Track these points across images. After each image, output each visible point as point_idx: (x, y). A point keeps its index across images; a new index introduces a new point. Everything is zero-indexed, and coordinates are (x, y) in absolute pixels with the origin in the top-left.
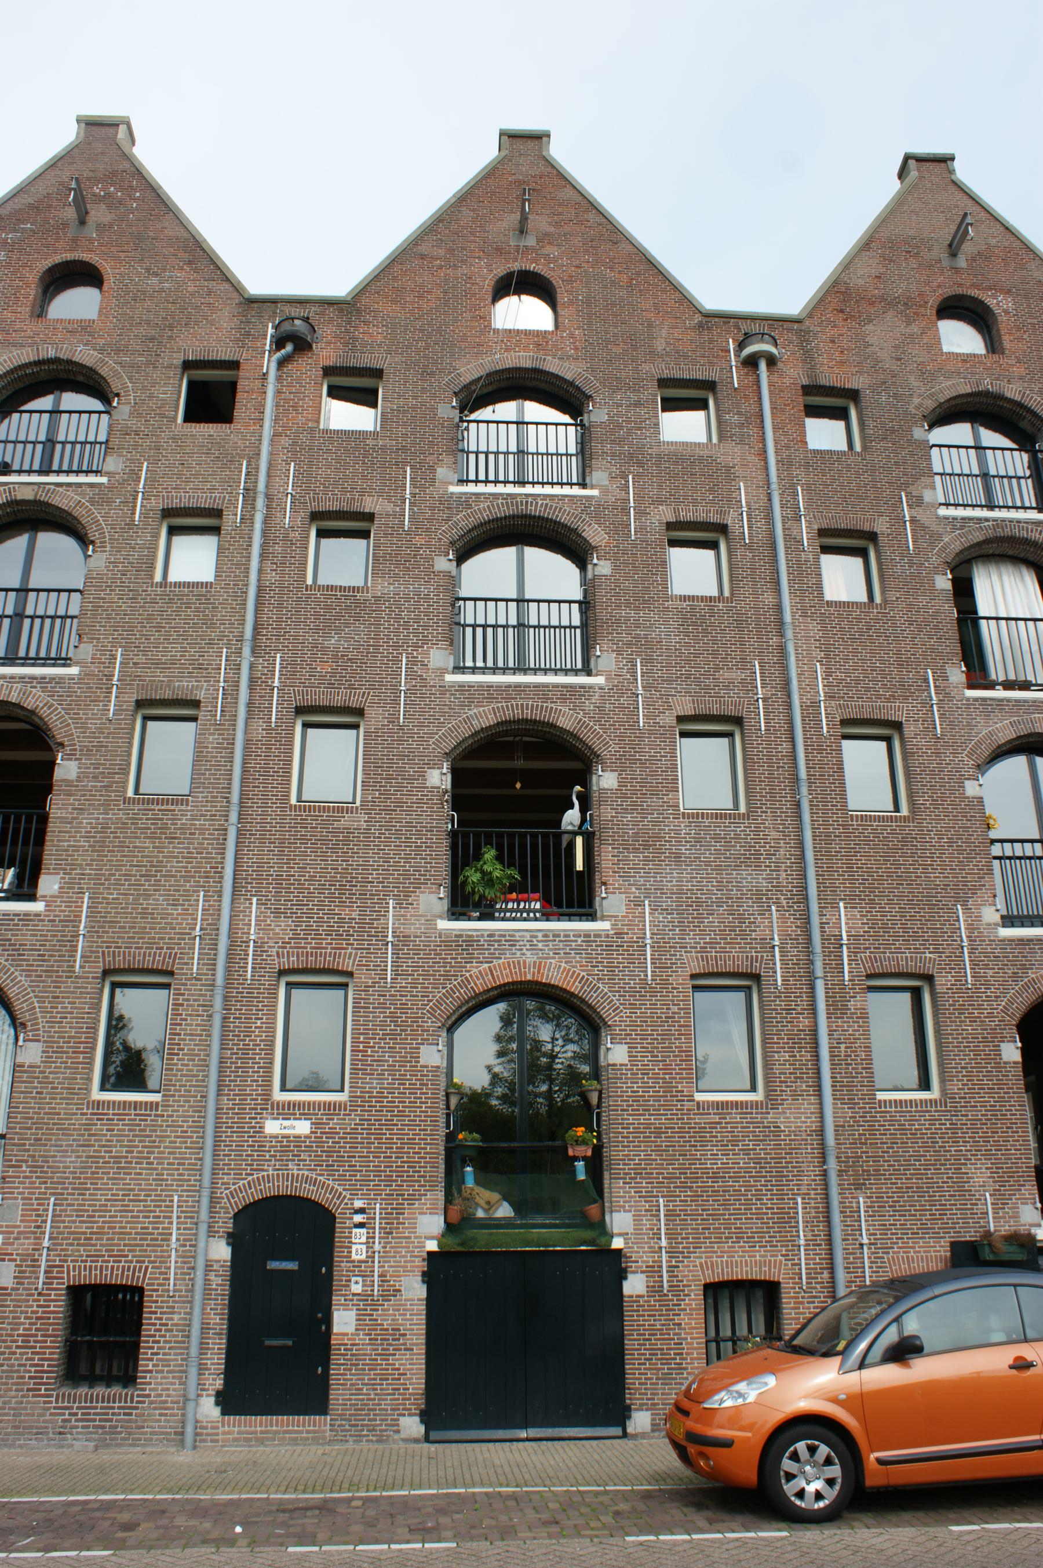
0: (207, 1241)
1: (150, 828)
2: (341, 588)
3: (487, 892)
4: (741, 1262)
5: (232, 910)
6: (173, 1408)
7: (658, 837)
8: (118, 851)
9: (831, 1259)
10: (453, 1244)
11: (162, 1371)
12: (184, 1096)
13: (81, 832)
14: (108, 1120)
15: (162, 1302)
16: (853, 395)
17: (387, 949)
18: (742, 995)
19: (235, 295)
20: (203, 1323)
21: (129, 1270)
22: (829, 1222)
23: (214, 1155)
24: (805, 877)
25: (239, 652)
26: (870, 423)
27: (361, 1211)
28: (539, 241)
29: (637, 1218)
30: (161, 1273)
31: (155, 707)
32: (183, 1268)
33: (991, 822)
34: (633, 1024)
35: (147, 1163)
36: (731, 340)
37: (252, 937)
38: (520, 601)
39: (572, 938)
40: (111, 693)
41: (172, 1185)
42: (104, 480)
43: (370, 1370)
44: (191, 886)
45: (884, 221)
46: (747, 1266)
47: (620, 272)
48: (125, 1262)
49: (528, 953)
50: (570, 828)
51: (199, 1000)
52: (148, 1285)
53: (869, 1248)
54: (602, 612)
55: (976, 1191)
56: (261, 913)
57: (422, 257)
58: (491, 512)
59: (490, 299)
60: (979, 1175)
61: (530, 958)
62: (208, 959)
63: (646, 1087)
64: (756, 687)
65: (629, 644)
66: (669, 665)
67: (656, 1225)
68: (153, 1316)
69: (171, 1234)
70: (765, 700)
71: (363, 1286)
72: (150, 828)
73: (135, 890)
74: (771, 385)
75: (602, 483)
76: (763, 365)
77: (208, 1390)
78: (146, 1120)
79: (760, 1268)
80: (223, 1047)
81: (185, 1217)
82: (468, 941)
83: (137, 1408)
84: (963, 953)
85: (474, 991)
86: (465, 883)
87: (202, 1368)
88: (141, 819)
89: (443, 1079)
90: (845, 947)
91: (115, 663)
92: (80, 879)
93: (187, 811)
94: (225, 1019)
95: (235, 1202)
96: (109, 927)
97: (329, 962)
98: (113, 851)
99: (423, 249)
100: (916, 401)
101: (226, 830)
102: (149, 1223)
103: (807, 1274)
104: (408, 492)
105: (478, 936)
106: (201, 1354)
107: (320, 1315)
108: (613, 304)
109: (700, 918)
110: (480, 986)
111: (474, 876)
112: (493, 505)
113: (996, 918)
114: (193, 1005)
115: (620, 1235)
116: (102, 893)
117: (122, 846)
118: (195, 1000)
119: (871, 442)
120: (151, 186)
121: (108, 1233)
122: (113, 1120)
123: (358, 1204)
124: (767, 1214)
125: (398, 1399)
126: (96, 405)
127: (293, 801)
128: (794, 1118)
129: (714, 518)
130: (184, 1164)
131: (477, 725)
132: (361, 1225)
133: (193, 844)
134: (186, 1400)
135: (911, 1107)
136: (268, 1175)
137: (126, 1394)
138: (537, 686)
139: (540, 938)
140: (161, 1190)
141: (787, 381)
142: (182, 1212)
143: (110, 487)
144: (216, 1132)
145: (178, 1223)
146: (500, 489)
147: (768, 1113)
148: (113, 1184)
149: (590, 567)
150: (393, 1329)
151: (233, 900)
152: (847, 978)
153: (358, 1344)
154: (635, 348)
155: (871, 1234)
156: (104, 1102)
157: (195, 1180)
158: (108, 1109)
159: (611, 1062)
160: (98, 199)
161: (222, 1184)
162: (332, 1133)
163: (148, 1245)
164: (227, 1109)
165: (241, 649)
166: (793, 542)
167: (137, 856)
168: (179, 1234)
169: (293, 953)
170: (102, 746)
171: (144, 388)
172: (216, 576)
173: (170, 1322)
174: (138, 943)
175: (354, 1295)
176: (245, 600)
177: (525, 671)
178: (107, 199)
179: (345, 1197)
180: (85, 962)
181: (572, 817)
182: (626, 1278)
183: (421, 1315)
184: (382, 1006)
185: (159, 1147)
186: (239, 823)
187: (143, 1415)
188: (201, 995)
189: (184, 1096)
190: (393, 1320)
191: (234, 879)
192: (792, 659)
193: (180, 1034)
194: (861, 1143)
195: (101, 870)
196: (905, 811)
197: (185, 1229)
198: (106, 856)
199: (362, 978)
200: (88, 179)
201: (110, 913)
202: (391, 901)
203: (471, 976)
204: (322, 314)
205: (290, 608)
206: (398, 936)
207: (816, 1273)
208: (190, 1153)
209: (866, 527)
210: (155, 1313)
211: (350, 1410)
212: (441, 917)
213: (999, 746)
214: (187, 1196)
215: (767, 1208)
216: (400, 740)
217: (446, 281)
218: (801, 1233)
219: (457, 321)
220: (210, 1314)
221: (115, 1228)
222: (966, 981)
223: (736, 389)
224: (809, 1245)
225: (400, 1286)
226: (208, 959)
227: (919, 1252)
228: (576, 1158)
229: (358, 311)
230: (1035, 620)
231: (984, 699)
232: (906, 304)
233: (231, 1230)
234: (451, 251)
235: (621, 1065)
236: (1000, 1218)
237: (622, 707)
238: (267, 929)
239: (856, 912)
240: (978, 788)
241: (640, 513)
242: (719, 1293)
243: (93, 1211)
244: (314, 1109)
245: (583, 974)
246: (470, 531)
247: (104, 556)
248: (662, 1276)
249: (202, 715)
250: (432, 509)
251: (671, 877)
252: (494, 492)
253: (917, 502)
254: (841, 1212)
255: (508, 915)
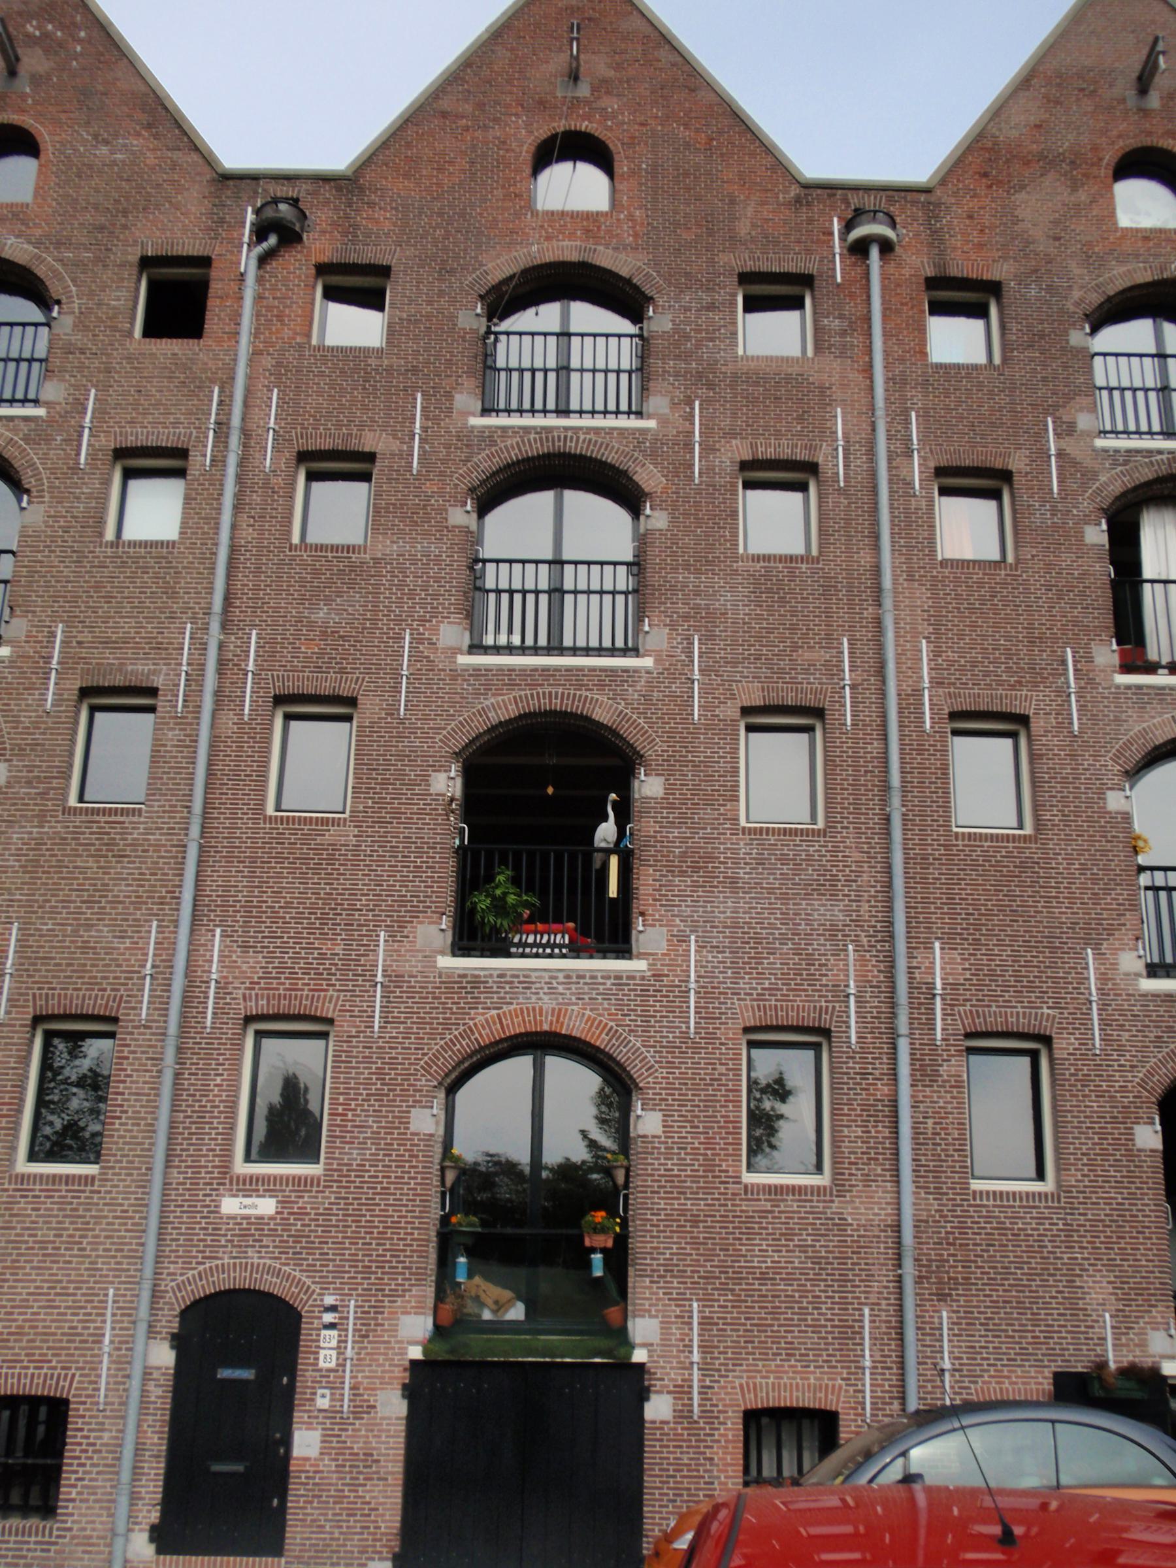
0: (147, 1344)
1: (93, 845)
2: (335, 548)
3: (499, 922)
4: (791, 1385)
5: (190, 943)
6: (99, 1545)
7: (710, 858)
8: (55, 873)
9: (903, 1386)
10: (442, 1352)
11: (87, 1501)
12: (126, 1168)
13: (9, 849)
14: (34, 1197)
15: (91, 1417)
16: (994, 288)
17: (375, 991)
18: (810, 1054)
19: (207, 169)
20: (137, 1444)
21: (52, 1379)
22: (902, 1340)
23: (159, 1240)
24: (890, 909)
25: (206, 628)
26: (1013, 326)
27: (333, 1309)
28: (594, 89)
29: (665, 1326)
30: (91, 1382)
31: (101, 696)
32: (116, 1376)
33: (1140, 844)
34: (670, 1087)
35: (79, 1249)
36: (835, 220)
37: (214, 976)
38: (557, 563)
39: (600, 980)
40: (49, 679)
41: (107, 1276)
42: (40, 412)
43: (334, 1503)
44: (142, 914)
45: (1051, 46)
46: (797, 1390)
47: (697, 131)
48: (49, 1368)
49: (546, 998)
50: (603, 845)
51: (147, 1052)
52: (74, 1396)
53: (953, 1376)
54: (654, 578)
55: (1093, 1310)
56: (226, 946)
57: (444, 115)
58: (520, 450)
59: (528, 170)
60: (1098, 1290)
61: (548, 1003)
62: (161, 1003)
63: (682, 1164)
64: (843, 671)
65: (686, 617)
66: (734, 643)
67: (688, 1335)
68: (79, 1434)
69: (103, 1335)
70: (853, 687)
71: (332, 1400)
72: (93, 845)
73: (75, 919)
74: (884, 277)
75: (661, 411)
76: (874, 252)
77: (141, 1523)
78: (79, 1197)
79: (815, 1393)
80: (175, 1108)
81: (122, 1315)
82: (476, 981)
83: (56, 1543)
84: (1091, 1009)
85: (479, 1043)
86: (473, 911)
87: (134, 1497)
88: (84, 833)
89: (438, 1149)
90: (938, 999)
91: (54, 642)
92: (8, 906)
93: (139, 823)
94: (177, 1075)
95: (183, 1297)
96: (42, 964)
97: (305, 1007)
98: (49, 873)
99: (445, 104)
100: (1076, 294)
101: (185, 846)
102: (79, 1321)
103: (872, 1403)
104: (418, 425)
105: (485, 976)
106: (134, 1480)
107: (278, 1435)
108: (686, 174)
109: (758, 958)
110: (486, 1036)
111: (483, 902)
112: (523, 441)
113: (1140, 966)
114: (140, 1059)
115: (644, 1345)
116: (34, 924)
117: (60, 865)
118: (143, 1052)
119: (1012, 350)
120: (98, 20)
121: (29, 1334)
122: (39, 1197)
123: (329, 1300)
124: (826, 1326)
125: (367, 1540)
126: (27, 310)
127: (270, 810)
128: (865, 1209)
129: (801, 455)
130: (122, 1250)
131: (494, 717)
132: (332, 1326)
133: (145, 863)
134: (115, 1535)
135: (1015, 1200)
136: (223, 1265)
137: (44, 1527)
138: (569, 669)
139: (561, 980)
140: (95, 1282)
141: (907, 272)
142: (118, 1308)
143: (50, 421)
144: (162, 1212)
145: (113, 1322)
146: (539, 421)
147: (832, 1201)
148: (37, 1275)
149: (642, 518)
150: (364, 1454)
151: (192, 931)
152: (939, 1036)
153: (322, 1472)
154: (710, 233)
155: (955, 1358)
156: (29, 1176)
157: (136, 1270)
158: (34, 1184)
159: (641, 1133)
160: (31, 41)
161: (169, 1274)
162: (301, 1214)
163: (76, 1348)
164: (178, 1184)
165: (208, 624)
166: (901, 485)
167: (78, 879)
168: (115, 1336)
169: (262, 996)
170: (37, 745)
171: (92, 294)
172: (181, 533)
173: (99, 1442)
174: (76, 983)
175: (320, 1411)
176: (214, 563)
177: (561, 650)
178: (45, 42)
179: (314, 1291)
180: (12, 1006)
181: (606, 832)
182: (648, 1399)
183: (399, 1437)
184: (367, 1060)
185: (94, 1230)
186: (202, 837)
187: (64, 1552)
188: (150, 1046)
189: (126, 1168)
190: (365, 1443)
191: (195, 905)
192: (890, 635)
193: (123, 1094)
194: (948, 1244)
195: (34, 895)
196: (1028, 830)
197: (121, 1329)
198: (40, 878)
199: (345, 1025)
200: (20, 14)
201: (43, 947)
202: (382, 933)
203: (475, 1025)
204: (315, 193)
205: (271, 569)
206: (390, 976)
207: (884, 1403)
208: (131, 1237)
209: (998, 464)
210: (81, 1430)
211: (310, 1551)
212: (443, 953)
213: (1156, 748)
214: (126, 1289)
215: (826, 1320)
216: (400, 736)
217: (474, 147)
218: (867, 1353)
219: (485, 201)
220: (146, 1432)
221: (37, 1327)
222: (1093, 1045)
223: (838, 285)
224: (876, 1368)
225: (376, 1401)
226: (161, 1003)
227: (1016, 1383)
228: (593, 1250)
229: (362, 190)
230: (1166, 582)
231: (1139, 687)
232: (1073, 162)
233: (175, 1331)
234: (480, 106)
235: (653, 1137)
236: (1122, 1345)
237: (673, 696)
238: (233, 966)
239: (955, 955)
240: (1123, 801)
241: (707, 449)
242: (762, 1424)
243: (12, 1307)
244: (281, 1184)
245: (611, 1024)
246: (494, 474)
247: (42, 508)
248: (691, 1399)
249: (161, 703)
250: (448, 446)
251: (725, 907)
252: (525, 427)
253: (1067, 430)
254: (918, 1328)
255: (528, 950)
